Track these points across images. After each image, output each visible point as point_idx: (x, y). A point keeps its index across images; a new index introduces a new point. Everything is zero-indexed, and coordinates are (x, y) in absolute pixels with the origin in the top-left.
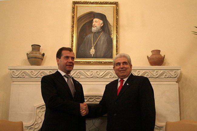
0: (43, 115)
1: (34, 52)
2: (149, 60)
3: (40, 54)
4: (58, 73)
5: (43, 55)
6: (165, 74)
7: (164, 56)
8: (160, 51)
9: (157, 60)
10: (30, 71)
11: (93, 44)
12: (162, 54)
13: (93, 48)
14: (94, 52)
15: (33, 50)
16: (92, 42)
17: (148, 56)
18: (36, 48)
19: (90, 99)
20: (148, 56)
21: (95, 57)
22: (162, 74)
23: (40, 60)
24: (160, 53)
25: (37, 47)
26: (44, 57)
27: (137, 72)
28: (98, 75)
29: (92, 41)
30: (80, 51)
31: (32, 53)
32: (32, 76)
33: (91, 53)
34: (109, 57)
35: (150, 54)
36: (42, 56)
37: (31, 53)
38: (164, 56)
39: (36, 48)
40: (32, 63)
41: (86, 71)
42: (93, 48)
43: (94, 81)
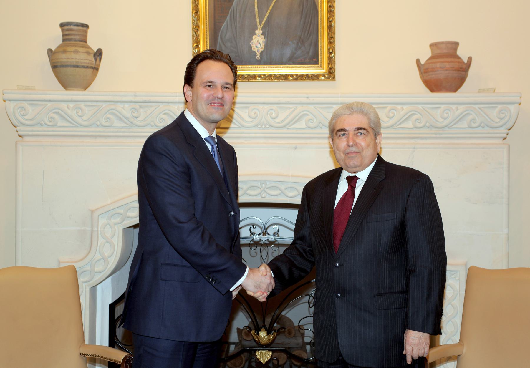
0: (102, 274)
1: (69, 49)
2: (421, 74)
3: (88, 53)
4: (123, 327)
5: (99, 54)
6: (470, 117)
7: (470, 59)
8: (457, 44)
9: (445, 71)
10: (71, 105)
11: (258, 20)
12: (463, 53)
13: (259, 32)
14: (263, 45)
15: (66, 38)
16: (256, 13)
17: (418, 61)
18: (74, 33)
19: (251, 188)
20: (418, 61)
21: (267, 59)
22: (461, 119)
23: (90, 71)
24: (456, 49)
25: (77, 30)
26: (100, 59)
27: (388, 109)
28: (273, 118)
29: (256, 9)
30: (219, 40)
31: (65, 52)
32: (79, 120)
33: (254, 49)
34: (308, 60)
35: (425, 55)
36: (96, 60)
37: (62, 49)
38: (470, 59)
39: (74, 33)
40: (433, 85)
41: (291, 125)
42: (259, 32)
43: (279, 151)
